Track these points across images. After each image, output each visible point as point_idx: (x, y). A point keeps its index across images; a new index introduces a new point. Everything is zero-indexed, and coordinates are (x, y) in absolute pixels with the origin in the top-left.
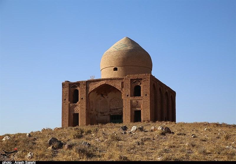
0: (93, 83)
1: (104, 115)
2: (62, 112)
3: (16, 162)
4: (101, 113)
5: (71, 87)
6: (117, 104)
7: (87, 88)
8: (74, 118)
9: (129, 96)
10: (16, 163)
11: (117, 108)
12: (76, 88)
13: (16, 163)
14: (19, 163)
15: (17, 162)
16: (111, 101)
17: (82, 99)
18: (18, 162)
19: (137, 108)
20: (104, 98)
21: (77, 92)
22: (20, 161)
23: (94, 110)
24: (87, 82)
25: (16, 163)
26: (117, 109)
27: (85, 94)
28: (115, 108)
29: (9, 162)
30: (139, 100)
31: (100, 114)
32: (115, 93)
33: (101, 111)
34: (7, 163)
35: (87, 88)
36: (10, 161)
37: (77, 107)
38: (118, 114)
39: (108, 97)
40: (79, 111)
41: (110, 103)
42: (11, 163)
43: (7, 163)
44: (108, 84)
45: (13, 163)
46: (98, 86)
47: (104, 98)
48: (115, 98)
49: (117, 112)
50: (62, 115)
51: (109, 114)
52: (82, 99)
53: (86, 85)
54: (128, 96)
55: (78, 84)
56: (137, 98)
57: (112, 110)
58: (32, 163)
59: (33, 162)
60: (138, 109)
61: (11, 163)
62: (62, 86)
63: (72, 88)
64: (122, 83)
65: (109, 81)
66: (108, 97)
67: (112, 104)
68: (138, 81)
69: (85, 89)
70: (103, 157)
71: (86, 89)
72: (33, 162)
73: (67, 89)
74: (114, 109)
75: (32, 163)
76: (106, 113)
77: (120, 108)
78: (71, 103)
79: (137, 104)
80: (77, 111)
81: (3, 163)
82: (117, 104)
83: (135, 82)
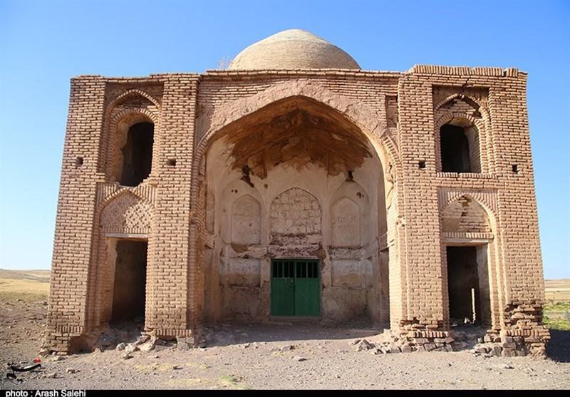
0: (233, 89)
1: (247, 257)
2: (58, 224)
3: (38, 393)
4: (234, 246)
5: (118, 104)
6: (304, 215)
7: (201, 113)
8: (119, 261)
9: (431, 167)
10: (38, 396)
11: (303, 231)
12: (142, 111)
13: (38, 396)
14: (47, 394)
15: (40, 391)
16: (277, 201)
17: (173, 163)
18: (42, 392)
19: (469, 235)
20: (252, 185)
21: (142, 135)
22: (49, 391)
23: (216, 232)
24: (202, 79)
25: (38, 396)
26: (301, 236)
27: (191, 139)
28: (294, 231)
29: (21, 393)
30: (479, 191)
31: (232, 250)
32: (299, 169)
33: (236, 241)
34: (18, 394)
35: (201, 113)
36: (23, 391)
37: (143, 207)
38: (306, 255)
39: (266, 186)
40: (152, 225)
41: (273, 208)
42: (25, 394)
43: (18, 394)
44: (315, 97)
45: (32, 394)
46: (262, 104)
47: (252, 185)
48: (292, 193)
49: (299, 247)
50: (56, 245)
51: (268, 254)
52: (173, 163)
53: (197, 98)
54: (422, 165)
55: (155, 87)
56: (465, 180)
57: (280, 239)
58: (76, 394)
59: (80, 392)
60: (472, 238)
61: (25, 394)
62: (72, 95)
63: (121, 109)
64: (391, 99)
65: (321, 82)
66: (266, 186)
67: (281, 216)
68: (467, 100)
69: (192, 112)
70: (36, 368)
71: (197, 116)
72: (80, 392)
73: (93, 110)
74: (291, 235)
75: (76, 394)
76: (257, 249)
77: (315, 233)
78: (108, 182)
79: (463, 214)
80: (140, 225)
81: (7, 396)
82: (304, 215)
83: (452, 102)
